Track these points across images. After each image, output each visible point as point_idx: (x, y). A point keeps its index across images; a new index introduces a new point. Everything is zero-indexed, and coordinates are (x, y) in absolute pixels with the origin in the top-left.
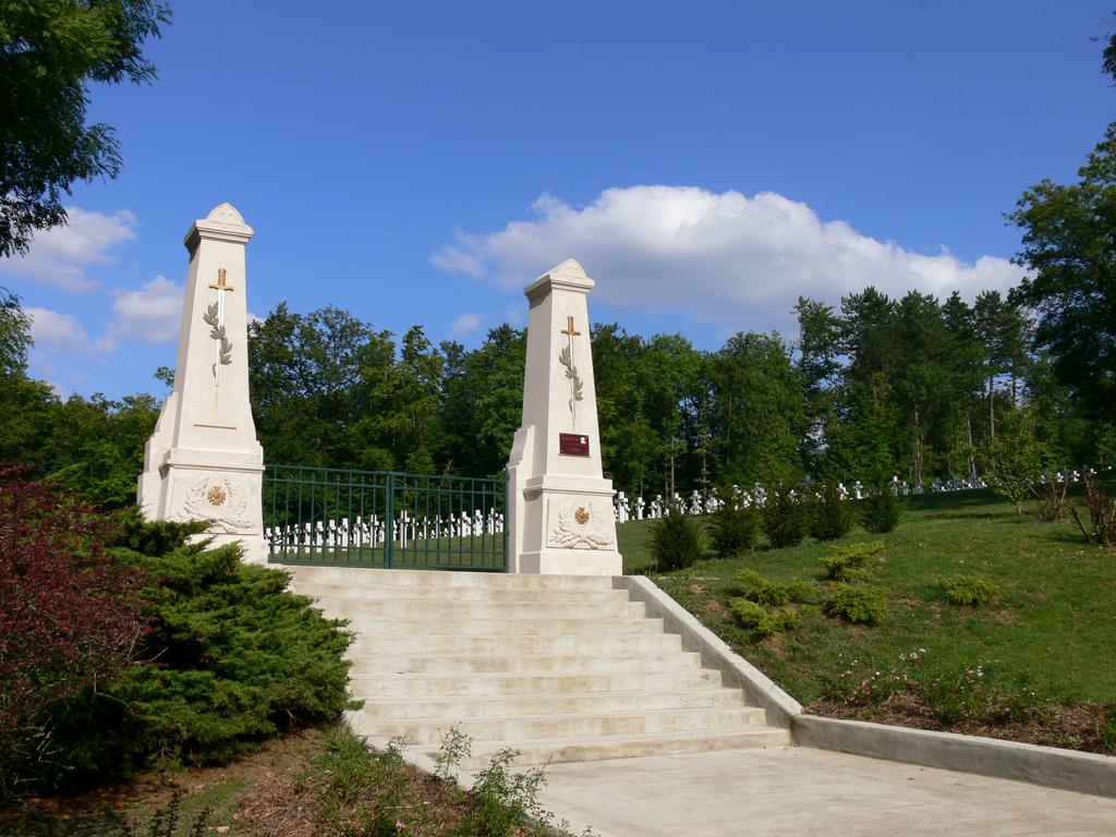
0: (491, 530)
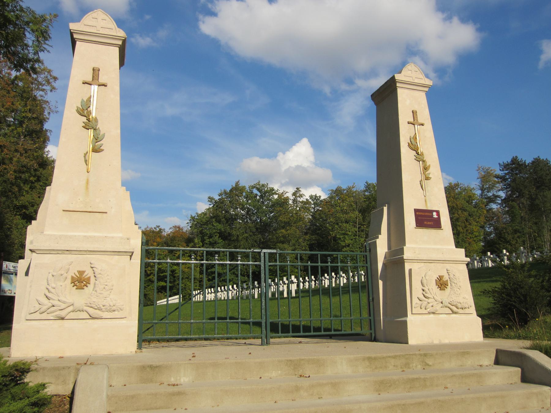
0: (43, 26)
